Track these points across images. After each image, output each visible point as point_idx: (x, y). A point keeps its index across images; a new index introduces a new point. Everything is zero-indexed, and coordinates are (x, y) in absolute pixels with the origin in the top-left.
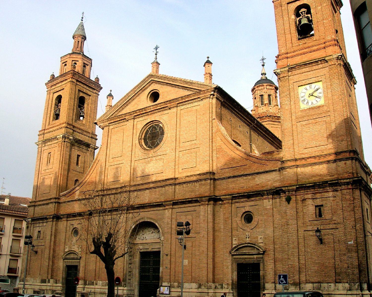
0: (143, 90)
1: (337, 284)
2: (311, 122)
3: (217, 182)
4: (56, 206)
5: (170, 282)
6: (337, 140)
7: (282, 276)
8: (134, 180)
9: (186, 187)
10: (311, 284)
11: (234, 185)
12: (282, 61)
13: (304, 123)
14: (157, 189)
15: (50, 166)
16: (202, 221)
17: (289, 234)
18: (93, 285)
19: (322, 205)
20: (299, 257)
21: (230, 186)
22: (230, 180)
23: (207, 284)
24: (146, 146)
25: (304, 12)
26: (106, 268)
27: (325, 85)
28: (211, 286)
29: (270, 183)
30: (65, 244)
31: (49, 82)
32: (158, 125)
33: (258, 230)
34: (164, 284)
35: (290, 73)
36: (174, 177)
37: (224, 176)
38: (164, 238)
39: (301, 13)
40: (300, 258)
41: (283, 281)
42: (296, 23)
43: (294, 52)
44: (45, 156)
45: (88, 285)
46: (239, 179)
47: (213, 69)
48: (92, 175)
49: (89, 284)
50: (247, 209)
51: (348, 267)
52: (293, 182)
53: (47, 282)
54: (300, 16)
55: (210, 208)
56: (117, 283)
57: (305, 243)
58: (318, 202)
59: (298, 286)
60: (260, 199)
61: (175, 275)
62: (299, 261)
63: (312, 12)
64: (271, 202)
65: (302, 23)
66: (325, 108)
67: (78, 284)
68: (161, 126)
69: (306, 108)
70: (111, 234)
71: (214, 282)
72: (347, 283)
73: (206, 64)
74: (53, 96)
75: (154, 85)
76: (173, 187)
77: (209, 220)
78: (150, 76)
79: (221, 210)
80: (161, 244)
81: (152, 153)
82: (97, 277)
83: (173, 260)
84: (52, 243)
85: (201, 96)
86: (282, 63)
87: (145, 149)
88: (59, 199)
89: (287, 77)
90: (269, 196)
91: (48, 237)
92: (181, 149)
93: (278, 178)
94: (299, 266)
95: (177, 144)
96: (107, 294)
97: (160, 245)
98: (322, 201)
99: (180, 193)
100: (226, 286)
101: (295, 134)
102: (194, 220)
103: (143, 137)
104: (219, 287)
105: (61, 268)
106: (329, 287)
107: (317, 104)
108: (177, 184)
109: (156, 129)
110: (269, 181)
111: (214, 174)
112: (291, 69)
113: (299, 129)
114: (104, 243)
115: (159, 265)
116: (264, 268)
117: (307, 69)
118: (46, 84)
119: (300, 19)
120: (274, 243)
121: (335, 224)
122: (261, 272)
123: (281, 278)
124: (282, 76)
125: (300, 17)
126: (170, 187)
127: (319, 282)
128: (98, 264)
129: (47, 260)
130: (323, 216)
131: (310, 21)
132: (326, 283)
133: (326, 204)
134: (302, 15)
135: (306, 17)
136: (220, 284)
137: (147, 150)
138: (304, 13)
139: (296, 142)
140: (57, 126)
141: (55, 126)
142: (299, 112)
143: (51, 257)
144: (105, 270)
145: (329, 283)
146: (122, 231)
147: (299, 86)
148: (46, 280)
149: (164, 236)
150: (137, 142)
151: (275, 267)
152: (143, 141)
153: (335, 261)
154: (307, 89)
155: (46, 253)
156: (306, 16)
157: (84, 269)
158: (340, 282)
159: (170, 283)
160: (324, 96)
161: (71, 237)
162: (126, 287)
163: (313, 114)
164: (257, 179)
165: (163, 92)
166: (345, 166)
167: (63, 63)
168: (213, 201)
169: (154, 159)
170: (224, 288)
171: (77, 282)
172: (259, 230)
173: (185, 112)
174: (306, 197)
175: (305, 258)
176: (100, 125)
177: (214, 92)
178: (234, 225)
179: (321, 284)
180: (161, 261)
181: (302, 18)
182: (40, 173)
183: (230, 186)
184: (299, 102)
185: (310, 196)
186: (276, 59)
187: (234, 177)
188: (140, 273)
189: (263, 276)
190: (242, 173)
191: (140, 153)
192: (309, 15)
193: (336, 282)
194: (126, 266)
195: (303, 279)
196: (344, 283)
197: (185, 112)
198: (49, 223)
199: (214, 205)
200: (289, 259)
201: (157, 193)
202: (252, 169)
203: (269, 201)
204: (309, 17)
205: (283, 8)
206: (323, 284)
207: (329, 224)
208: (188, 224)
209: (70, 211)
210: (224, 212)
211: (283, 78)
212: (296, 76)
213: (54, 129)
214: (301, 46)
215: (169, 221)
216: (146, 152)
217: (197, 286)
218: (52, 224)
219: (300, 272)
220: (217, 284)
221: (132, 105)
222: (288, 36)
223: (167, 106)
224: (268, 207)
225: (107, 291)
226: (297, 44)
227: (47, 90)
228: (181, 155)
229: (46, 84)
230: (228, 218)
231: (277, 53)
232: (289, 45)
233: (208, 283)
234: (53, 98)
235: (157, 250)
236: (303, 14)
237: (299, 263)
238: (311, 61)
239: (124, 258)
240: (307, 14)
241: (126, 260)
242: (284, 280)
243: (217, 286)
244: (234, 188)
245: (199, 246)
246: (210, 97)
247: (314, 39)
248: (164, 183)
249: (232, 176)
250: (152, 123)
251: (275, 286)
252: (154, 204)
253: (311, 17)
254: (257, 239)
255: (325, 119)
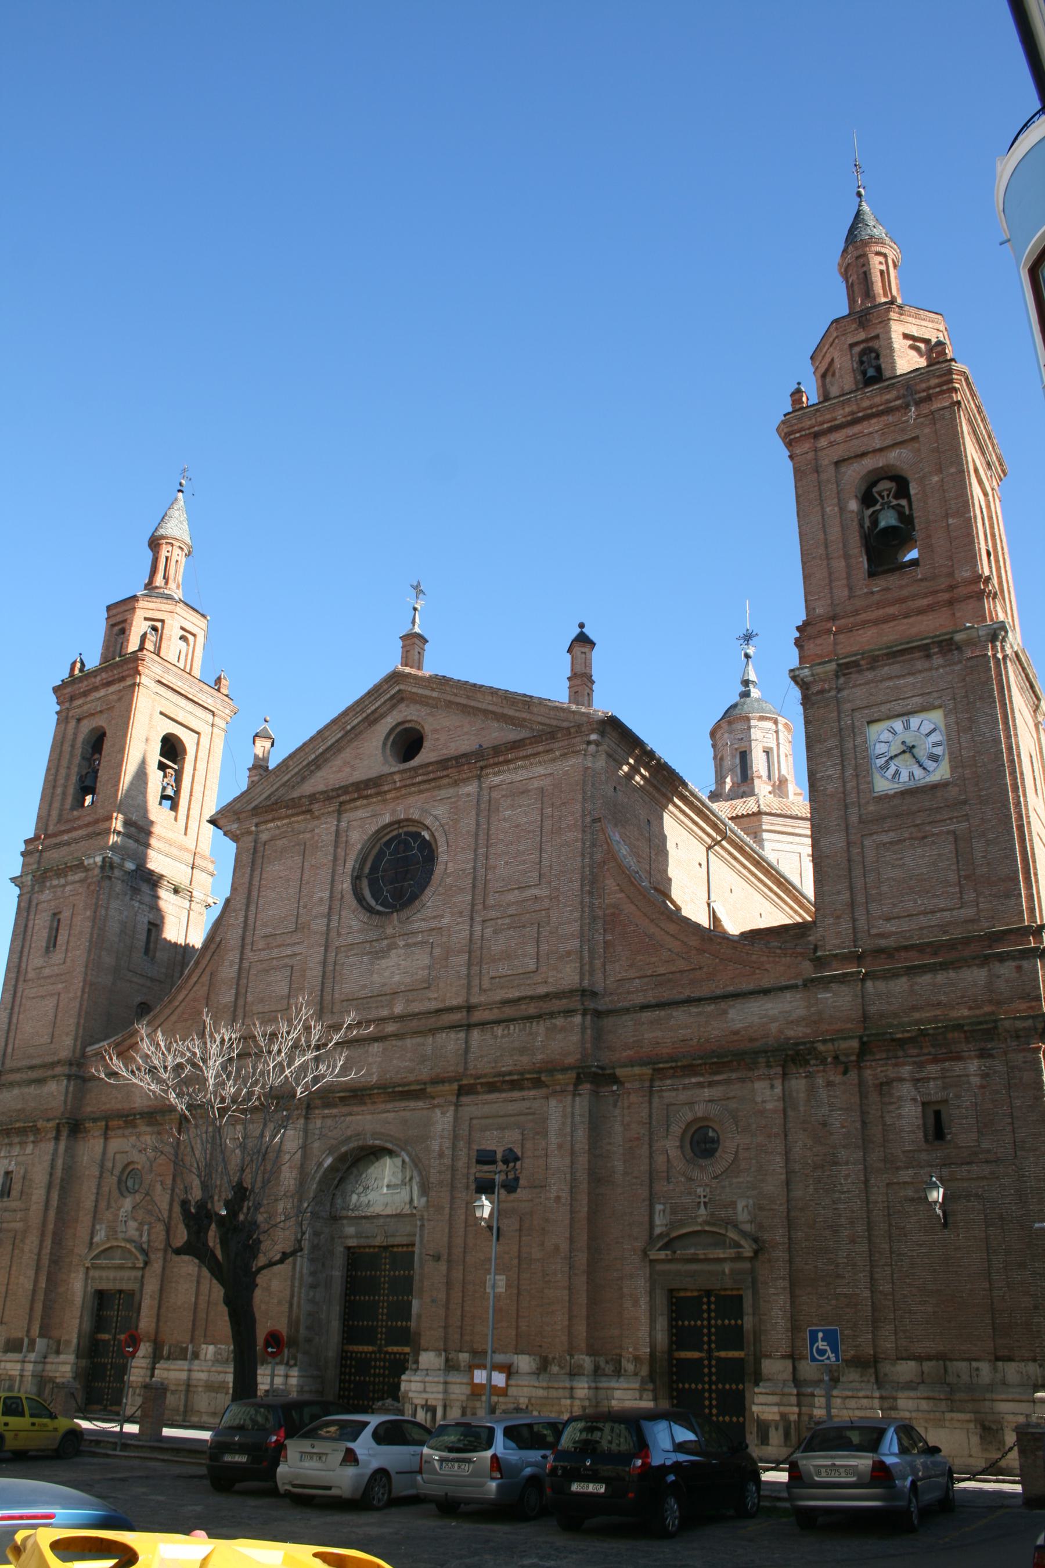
0: (372, 720)
1: (1000, 1364)
2: (906, 835)
3: (608, 1022)
4: (71, 1089)
5: (445, 1350)
6: (990, 895)
7: (820, 1335)
8: (335, 1010)
9: (503, 1036)
10: (912, 1364)
11: (659, 1034)
12: (819, 641)
13: (885, 838)
14: (409, 1042)
15: (58, 956)
16: (553, 1147)
17: (837, 1195)
18: (185, 1359)
19: (945, 1101)
20: (871, 1273)
21: (646, 1036)
22: (647, 1015)
23: (568, 1358)
24: (377, 901)
25: (887, 490)
26: (228, 1301)
27: (952, 719)
28: (580, 1366)
29: (774, 1027)
30: (94, 1217)
31: (64, 684)
32: (417, 836)
33: (735, 1180)
34: (819, 1413)
35: (841, 680)
36: (465, 1004)
37: (626, 1004)
38: (428, 1201)
39: (880, 493)
40: (876, 1276)
41: (825, 1351)
42: (862, 526)
43: (856, 613)
44: (41, 922)
45: (168, 1358)
46: (675, 1014)
47: (600, 662)
48: (195, 989)
49: (170, 1353)
50: (700, 1110)
51: (1036, 1307)
52: (849, 1026)
53: (25, 1349)
54: (875, 502)
55: (581, 1105)
56: (270, 1350)
57: (890, 1225)
58: (933, 1090)
59: (872, 1370)
60: (742, 1080)
61: (461, 1328)
62: (872, 1285)
63: (912, 492)
64: (778, 1090)
65: (882, 524)
66: (953, 792)
67: (133, 1355)
68: (427, 837)
69: (892, 792)
70: (246, 1189)
71: (592, 1352)
72: (1034, 1360)
73: (575, 644)
74: (77, 728)
75: (407, 706)
76: (462, 1035)
77: (577, 1146)
78: (395, 677)
79: (617, 1112)
80: (419, 1223)
81: (393, 925)
82: (199, 1332)
83: (457, 1275)
84: (52, 1214)
85: (557, 745)
86: (822, 646)
87: (369, 910)
88: (80, 1065)
89: (833, 693)
90: (772, 1071)
91: (38, 1194)
92: (493, 914)
93: (801, 1012)
94: (873, 1302)
95: (479, 899)
96: (231, 1391)
97: (416, 1226)
98: (944, 1088)
99: (481, 1056)
100: (630, 1367)
101: (857, 872)
102: (529, 1145)
103: (367, 870)
104: (609, 1369)
105: (78, 1300)
106: (974, 1374)
107: (928, 779)
108: (476, 1025)
109: (408, 847)
110: (774, 1020)
111: (594, 994)
112: (846, 668)
113: (870, 855)
114: (221, 1221)
115: (410, 1291)
116: (755, 1306)
117: (895, 669)
118: (56, 690)
119: (874, 512)
120: (790, 1224)
121: (987, 1162)
122: (746, 1318)
123: (817, 1341)
124: (815, 689)
125: (874, 505)
126: (453, 1035)
127: (942, 1357)
128: (205, 1287)
129: (31, 1273)
130: (949, 1137)
131: (907, 520)
132: (964, 1360)
133: (958, 1097)
134: (881, 500)
135: (893, 507)
136: (612, 1360)
137: (379, 913)
138: (888, 496)
139: (861, 899)
140: (87, 825)
141: (80, 827)
142: (868, 802)
143: (45, 1261)
144: (226, 1309)
145: (975, 1360)
146: (288, 1177)
147: (869, 723)
148: (22, 1340)
149: (427, 1196)
150: (347, 886)
151: (792, 1303)
152: (365, 883)
153: (991, 1284)
154: (895, 733)
155: (27, 1249)
156: (895, 502)
157: (156, 1302)
158: (1010, 1359)
159: (443, 1354)
160: (950, 754)
161: (115, 1193)
162: (295, 1365)
163: (914, 808)
164: (732, 1014)
165: (435, 731)
166: (1017, 975)
167: (113, 625)
168: (592, 1083)
169: (401, 943)
170: (625, 1371)
171: (131, 1350)
172: (741, 1180)
173: (503, 796)
174: (892, 1073)
175: (892, 1274)
176: (228, 828)
177: (602, 734)
178: (660, 1160)
179: (948, 1363)
180: (416, 1278)
181: (881, 510)
182: (21, 978)
183: (646, 1036)
184: (869, 773)
185: (906, 1071)
186: (797, 635)
187: (660, 1006)
188: (345, 1320)
189: (755, 1332)
190: (687, 993)
191: (355, 924)
192: (904, 502)
193: (998, 1359)
194: (300, 1293)
195: (888, 1344)
196: (1023, 1361)
197: (503, 796)
198: (42, 1145)
199: (595, 1093)
200: (839, 1276)
201: (409, 1055)
202: (719, 981)
203: (772, 1087)
204: (903, 507)
205: (824, 476)
206: (955, 1363)
207: (968, 1163)
208: (511, 1158)
209: (119, 1106)
210: (627, 1119)
211: (819, 697)
212: (857, 693)
213: (75, 834)
214: (877, 597)
215: (447, 1144)
216: (376, 920)
217: (534, 1366)
218: (56, 1150)
219: (875, 1323)
220: (602, 1361)
221: (334, 769)
222: (839, 565)
223: (447, 776)
224: (769, 1106)
225: (230, 1378)
226: (865, 590)
227: (58, 708)
228: (488, 932)
229: (56, 690)
230: (638, 1139)
231: (801, 617)
232: (842, 593)
233: (572, 1356)
234: (75, 734)
235: (404, 1240)
236: (882, 497)
237: (872, 1292)
238: (908, 643)
239: (294, 1268)
240: (896, 497)
241: (301, 1272)
242: (828, 1348)
243: (602, 1364)
244: (658, 1043)
245: (543, 1229)
246: (586, 750)
247: (919, 576)
248: (432, 1022)
249: (653, 1001)
250: (396, 826)
251: (794, 1368)
252: (397, 1089)
253: (911, 508)
254: (735, 1208)
255: (952, 827)
